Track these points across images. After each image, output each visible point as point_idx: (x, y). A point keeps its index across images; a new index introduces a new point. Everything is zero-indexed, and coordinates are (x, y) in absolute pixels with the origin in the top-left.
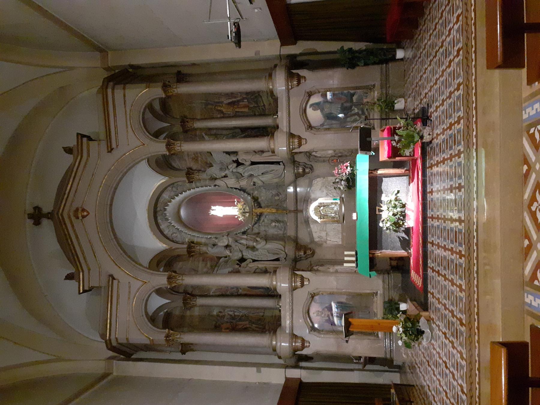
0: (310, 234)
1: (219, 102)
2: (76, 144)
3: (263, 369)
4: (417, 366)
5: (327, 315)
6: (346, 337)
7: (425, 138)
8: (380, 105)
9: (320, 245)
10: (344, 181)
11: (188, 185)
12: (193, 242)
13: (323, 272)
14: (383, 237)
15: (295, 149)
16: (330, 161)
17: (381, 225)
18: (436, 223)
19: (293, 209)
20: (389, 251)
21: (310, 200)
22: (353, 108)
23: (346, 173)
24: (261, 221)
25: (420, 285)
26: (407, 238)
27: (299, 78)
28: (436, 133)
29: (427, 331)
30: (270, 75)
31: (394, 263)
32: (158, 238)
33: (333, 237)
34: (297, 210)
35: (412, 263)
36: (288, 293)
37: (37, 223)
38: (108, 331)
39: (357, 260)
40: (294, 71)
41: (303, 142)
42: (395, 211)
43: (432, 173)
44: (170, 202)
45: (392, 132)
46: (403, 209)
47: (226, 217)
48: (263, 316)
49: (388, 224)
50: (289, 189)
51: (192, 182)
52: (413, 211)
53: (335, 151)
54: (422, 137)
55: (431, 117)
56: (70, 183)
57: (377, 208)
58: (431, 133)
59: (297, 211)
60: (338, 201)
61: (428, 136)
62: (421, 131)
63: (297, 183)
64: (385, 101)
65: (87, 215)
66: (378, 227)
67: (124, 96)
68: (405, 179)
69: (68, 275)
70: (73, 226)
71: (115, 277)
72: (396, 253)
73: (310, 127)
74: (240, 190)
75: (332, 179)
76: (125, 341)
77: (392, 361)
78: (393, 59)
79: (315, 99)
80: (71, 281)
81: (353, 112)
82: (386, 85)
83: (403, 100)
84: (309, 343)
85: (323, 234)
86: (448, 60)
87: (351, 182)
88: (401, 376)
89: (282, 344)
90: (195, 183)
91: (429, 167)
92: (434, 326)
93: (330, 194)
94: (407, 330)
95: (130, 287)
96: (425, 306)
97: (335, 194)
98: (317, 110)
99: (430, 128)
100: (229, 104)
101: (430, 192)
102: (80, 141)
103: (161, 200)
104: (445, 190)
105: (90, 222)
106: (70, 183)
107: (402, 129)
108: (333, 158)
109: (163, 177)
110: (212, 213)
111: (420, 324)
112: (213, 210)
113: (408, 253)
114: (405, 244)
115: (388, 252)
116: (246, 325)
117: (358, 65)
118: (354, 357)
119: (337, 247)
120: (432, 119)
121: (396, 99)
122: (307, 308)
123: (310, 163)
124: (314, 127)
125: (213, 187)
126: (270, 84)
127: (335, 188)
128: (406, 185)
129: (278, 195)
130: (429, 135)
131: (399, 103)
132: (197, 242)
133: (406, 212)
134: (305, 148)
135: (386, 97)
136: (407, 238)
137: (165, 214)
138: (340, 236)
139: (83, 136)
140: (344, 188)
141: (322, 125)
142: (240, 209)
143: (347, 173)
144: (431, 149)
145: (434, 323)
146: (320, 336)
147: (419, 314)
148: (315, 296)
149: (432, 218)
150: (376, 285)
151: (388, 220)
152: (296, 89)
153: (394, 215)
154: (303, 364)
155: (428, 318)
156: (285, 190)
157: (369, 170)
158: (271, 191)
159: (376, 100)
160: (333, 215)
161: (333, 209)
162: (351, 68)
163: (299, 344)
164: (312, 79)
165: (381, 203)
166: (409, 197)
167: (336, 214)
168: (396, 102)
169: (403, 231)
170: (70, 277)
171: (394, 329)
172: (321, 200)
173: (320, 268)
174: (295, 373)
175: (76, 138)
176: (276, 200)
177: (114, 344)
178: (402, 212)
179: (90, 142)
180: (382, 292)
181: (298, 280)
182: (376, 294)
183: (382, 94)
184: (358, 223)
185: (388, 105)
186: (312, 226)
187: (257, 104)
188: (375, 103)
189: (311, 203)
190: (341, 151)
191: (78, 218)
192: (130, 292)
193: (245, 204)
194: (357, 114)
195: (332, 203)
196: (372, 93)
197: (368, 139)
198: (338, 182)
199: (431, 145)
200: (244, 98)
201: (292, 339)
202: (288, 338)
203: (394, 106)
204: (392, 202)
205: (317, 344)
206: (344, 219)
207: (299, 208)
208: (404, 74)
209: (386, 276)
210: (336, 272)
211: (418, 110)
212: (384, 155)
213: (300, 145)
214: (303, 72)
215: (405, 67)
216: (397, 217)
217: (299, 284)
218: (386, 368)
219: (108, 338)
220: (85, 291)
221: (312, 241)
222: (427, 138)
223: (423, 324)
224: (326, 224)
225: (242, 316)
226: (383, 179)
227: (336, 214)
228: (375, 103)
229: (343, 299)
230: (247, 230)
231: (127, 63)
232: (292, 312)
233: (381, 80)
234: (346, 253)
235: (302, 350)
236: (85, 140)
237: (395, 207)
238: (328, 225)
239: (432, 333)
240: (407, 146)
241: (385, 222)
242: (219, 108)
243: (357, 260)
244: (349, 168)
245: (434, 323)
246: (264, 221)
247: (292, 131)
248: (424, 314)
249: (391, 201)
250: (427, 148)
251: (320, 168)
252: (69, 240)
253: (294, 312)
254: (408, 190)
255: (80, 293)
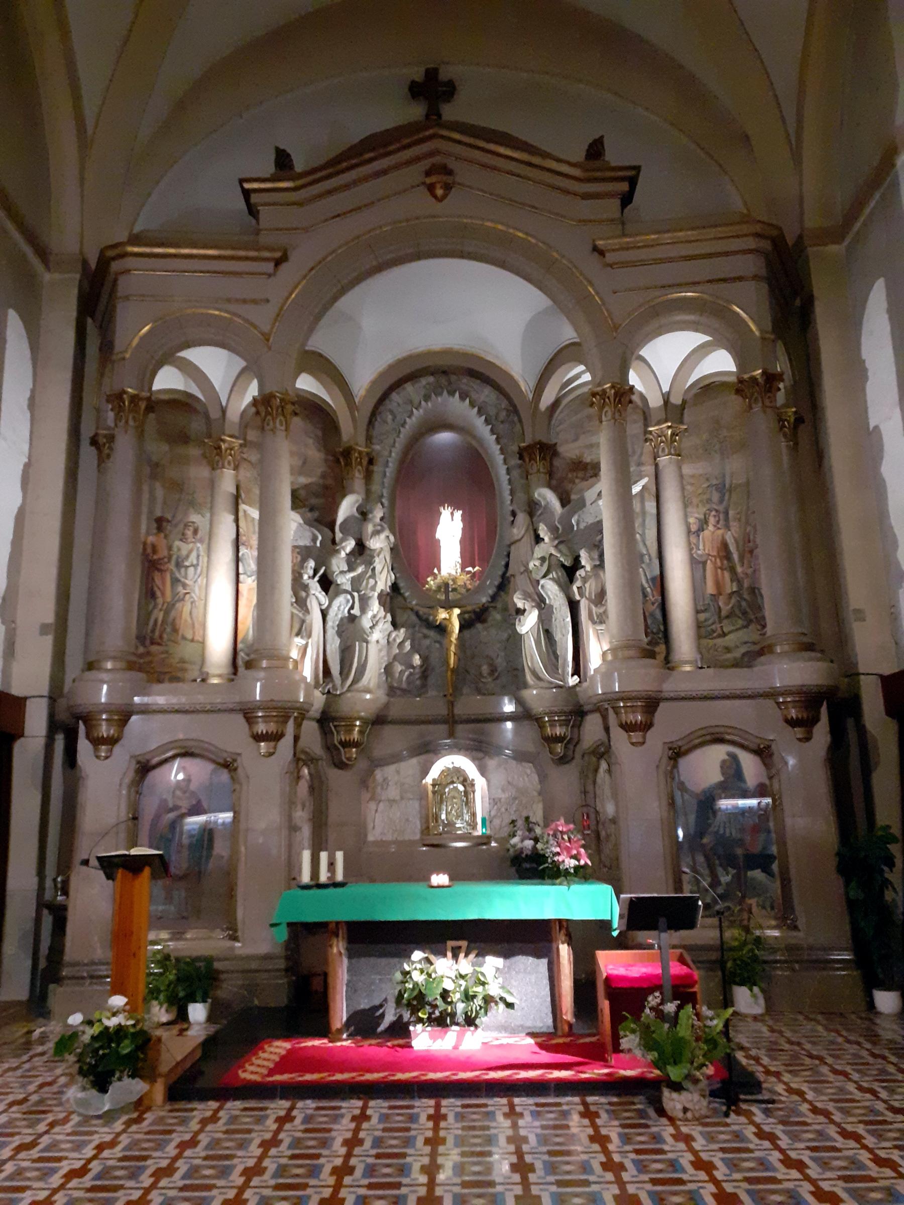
0: (395, 759)
1: (727, 519)
2: (613, 164)
3: (49, 640)
4: (25, 1058)
5: (180, 803)
6: (100, 859)
7: (675, 1095)
8: (745, 943)
9: (365, 781)
10: (534, 848)
11: (515, 448)
12: (371, 462)
13: (293, 792)
14: (383, 961)
15: (617, 713)
16: (585, 810)
17: (417, 955)
18: (424, 1125)
19: (456, 711)
20: (346, 977)
21: (480, 755)
22: (733, 871)
23: (558, 854)
24: (425, 631)
25: (243, 1075)
26: (381, 1028)
27: (804, 724)
28: (688, 1120)
29: (106, 1103)
30: (809, 647)
31: (316, 984)
32: (382, 376)
33: (387, 819)
34: (455, 722)
35: (310, 1043)
36: (237, 699)
37: (416, 91)
38: (147, 250)
39: (320, 886)
40: (824, 710)
41: (636, 736)
42: (455, 997)
43: (565, 1114)
44: (472, 404)
45: (683, 992)
46: (460, 1018)
47: (434, 547)
48: (184, 638)
49: (418, 977)
50: (510, 701)
51: (521, 457)
52: (456, 1047)
53: (614, 821)
54: (677, 1087)
55: (738, 1113)
56: (516, 155)
57: (464, 944)
58: (689, 1115)
59: (451, 722)
60: (479, 831)
61: (679, 1106)
62: (696, 1081)
63: (526, 722)
64: (755, 959)
65: (435, 197)
66: (412, 946)
67: (740, 279)
68: (545, 1022)
69: (288, 155)
70: (408, 163)
71: (284, 267)
72: (338, 997)
73: (676, 754)
74: (503, 576)
75: (537, 815)
76: (121, 290)
77: (58, 980)
78: (872, 981)
79: (750, 764)
80: (273, 165)
81: (720, 870)
82: (797, 962)
83: (759, 1009)
84: (107, 758)
85: (393, 792)
86: (831, 1107)
87: (533, 867)
88: (19, 1003)
89: (105, 687)
90: (520, 466)
91: (585, 1104)
92: (118, 1126)
93: (499, 810)
94: (110, 1041)
95: (255, 302)
96: (185, 1088)
97: (497, 822)
98: (723, 774)
99: (704, 1112)
100: (725, 546)
101: (512, 1106)
102: (621, 174)
103: (475, 384)
104: (517, 1141)
105: (420, 203)
106: (516, 155)
107: (696, 1023)
108: (592, 816)
109: (533, 389)
110: (445, 513)
111: (127, 1081)
112: (452, 514)
113: (340, 1031)
114: (364, 1023)
115: (341, 973)
116: (163, 594)
117: (847, 884)
118: (68, 877)
119: (361, 830)
120: (733, 1115)
121: (763, 991)
122: (197, 751)
123: (578, 756)
124: (675, 766)
125: (511, 508)
126: (786, 648)
127: (513, 822)
128: (529, 1023)
129: (493, 670)
130: (685, 1110)
131: (751, 1000)
132: (372, 472)
133: (454, 1028)
134: (620, 740)
135: (765, 962)
136: (381, 1028)
137: (441, 394)
138: (389, 837)
139: (633, 182)
140: (514, 846)
141: (682, 787)
142: (454, 580)
143: (560, 858)
144: (642, 1114)
145: (128, 1124)
146: (125, 786)
147: (160, 1075)
148: (230, 771)
149: (437, 1118)
150: (258, 939)
151: (429, 975)
152: (778, 714)
153: (445, 994)
154: (60, 742)
155: (146, 1102)
156: (505, 690)
157: (567, 920)
158: (503, 654)
159: (758, 933)
160: (443, 817)
161: (460, 816)
162: (839, 863)
163: (104, 730)
164: (803, 760)
165: (477, 956)
166: (495, 1034)
167: (445, 826)
168: (756, 989)
169: (401, 1017)
170: (283, 160)
171: (118, 1001)
172: (480, 783)
173: (303, 787)
174: (36, 721)
175: (627, 164)
176: (480, 667)
177: (115, 266)
178: (453, 1015)
179: (617, 202)
180: (238, 952)
181: (272, 727)
182: (234, 938)
183: (774, 951)
184: (418, 888)
185: (734, 968)
186: (414, 761)
187: (727, 617)
188: (747, 930)
189: (473, 760)
190: (613, 838)
191: (428, 174)
192: (245, 301)
193: (468, 590)
194: (715, 883)
195: (474, 815)
196: (773, 923)
197: (662, 921)
198: (530, 830)
199: (651, 1112)
200: (740, 582)
201: (118, 712)
202: (118, 701)
203: (741, 984)
204: (480, 989)
205: (103, 780)
206: (430, 849)
207: (460, 728)
208: (831, 1014)
209: (282, 964)
210: (293, 828)
211: (744, 1061)
212: (612, 963)
213: (628, 727)
214: (822, 732)
215: (853, 1017)
216: (440, 1002)
217: (261, 728)
218: (42, 964)
219: (130, 249)
220: (247, 194)
221: (377, 763)
222: (673, 1101)
223: (125, 1088)
224: (421, 799)
225: (185, 586)
226: (544, 961)
227: (445, 826)
228: (747, 930)
229: (221, 848)
230: (401, 595)
231: (816, 292)
232: (186, 712)
233: (811, 948)
234: (339, 855)
235: (88, 737)
236: (624, 187)
237: (468, 997)
238: (416, 804)
239: (99, 1117)
240: (649, 1044)
241: (423, 965)
242: (712, 520)
243: (320, 886)
244: (573, 863)
245: (128, 1124)
246: (425, 637)
247: (662, 705)
248: (159, 1091)
249: (483, 984)
250: (641, 1098)
251: (565, 782)
252: (371, 155)
253: (188, 717)
254: (512, 1030)
255: (241, 181)
